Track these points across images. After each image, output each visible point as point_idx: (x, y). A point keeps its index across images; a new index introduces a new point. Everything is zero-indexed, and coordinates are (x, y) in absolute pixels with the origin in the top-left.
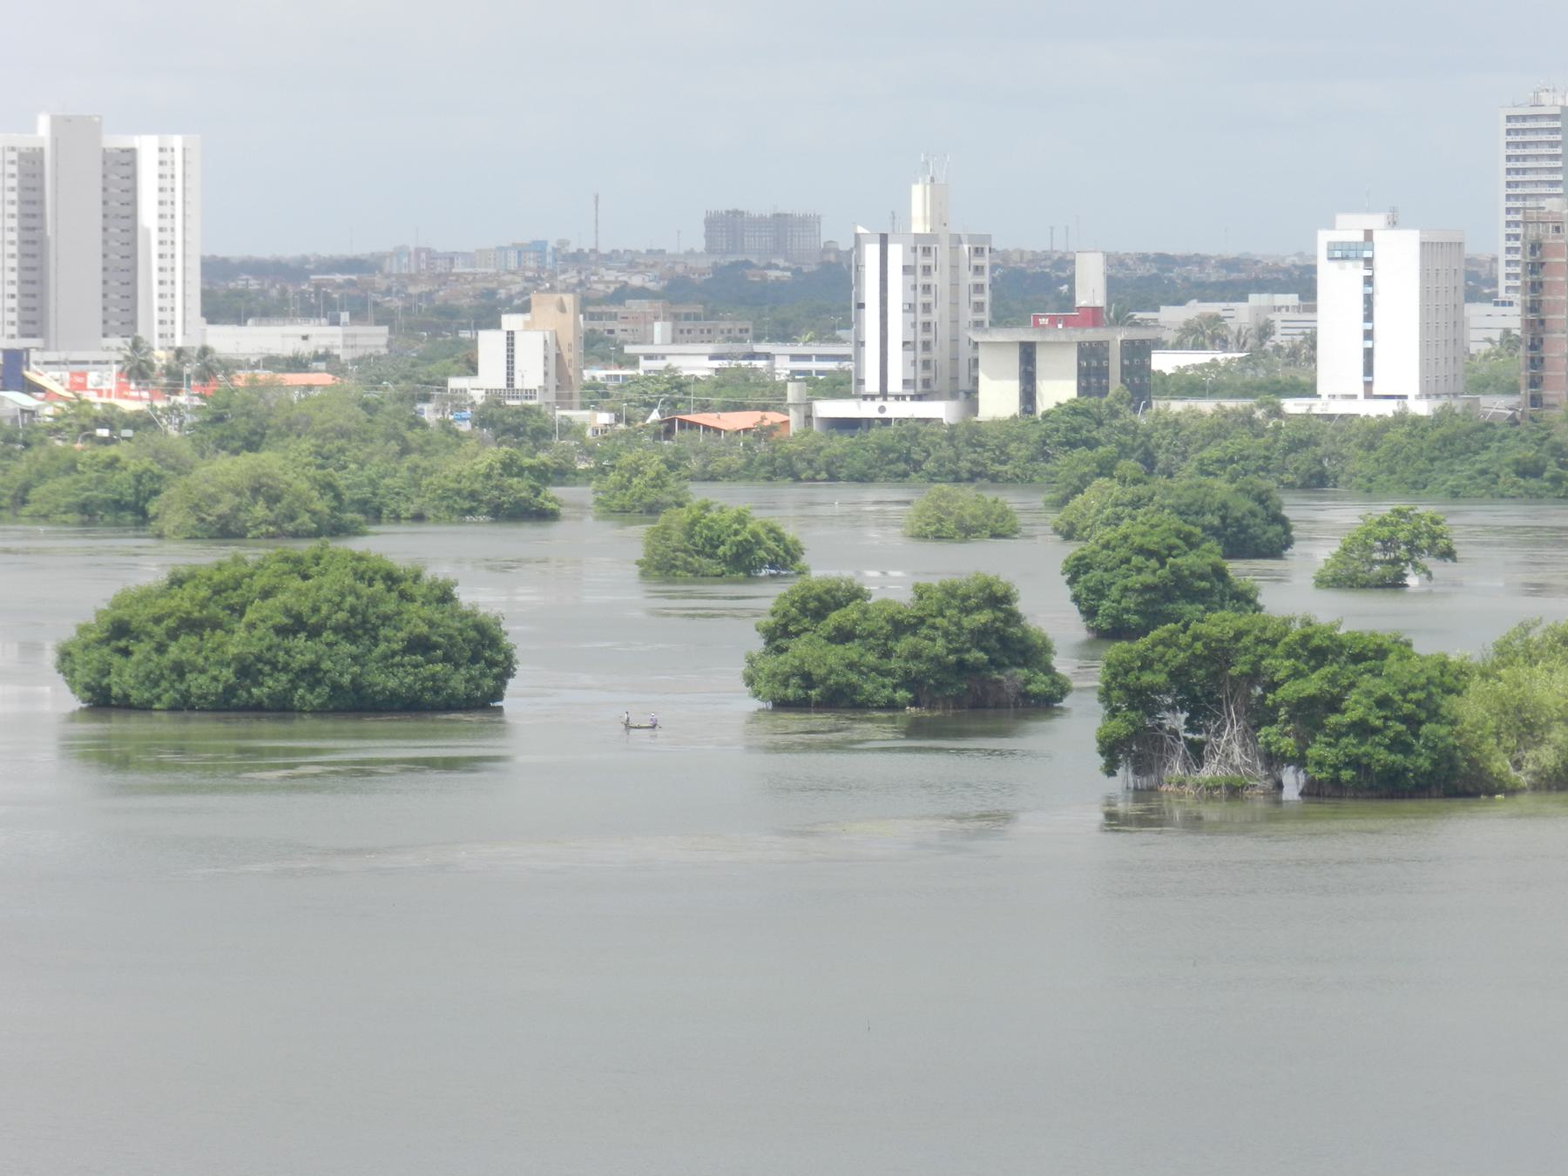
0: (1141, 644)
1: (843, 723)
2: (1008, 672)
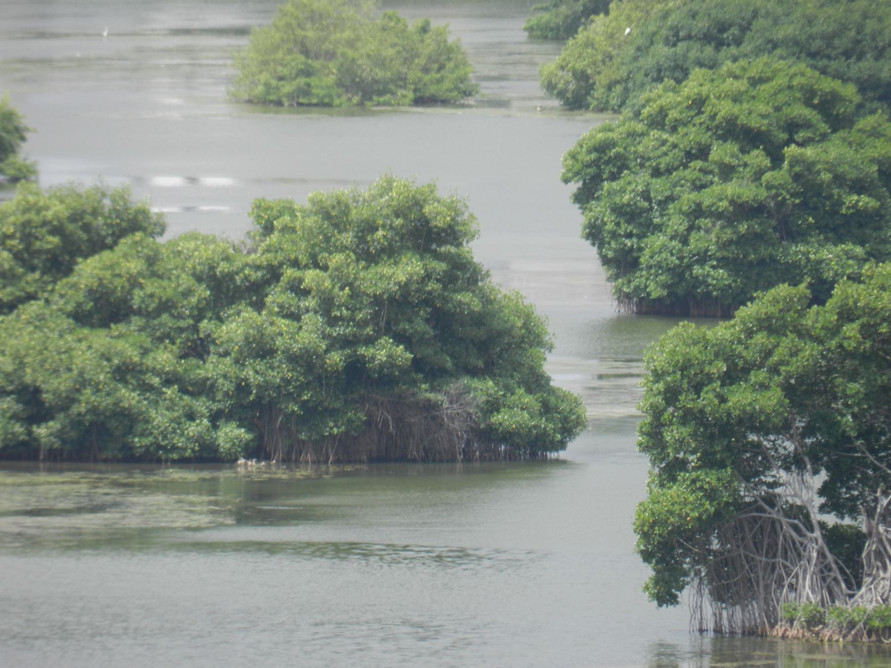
0: (721, 332)
1: (105, 493)
2: (454, 387)
